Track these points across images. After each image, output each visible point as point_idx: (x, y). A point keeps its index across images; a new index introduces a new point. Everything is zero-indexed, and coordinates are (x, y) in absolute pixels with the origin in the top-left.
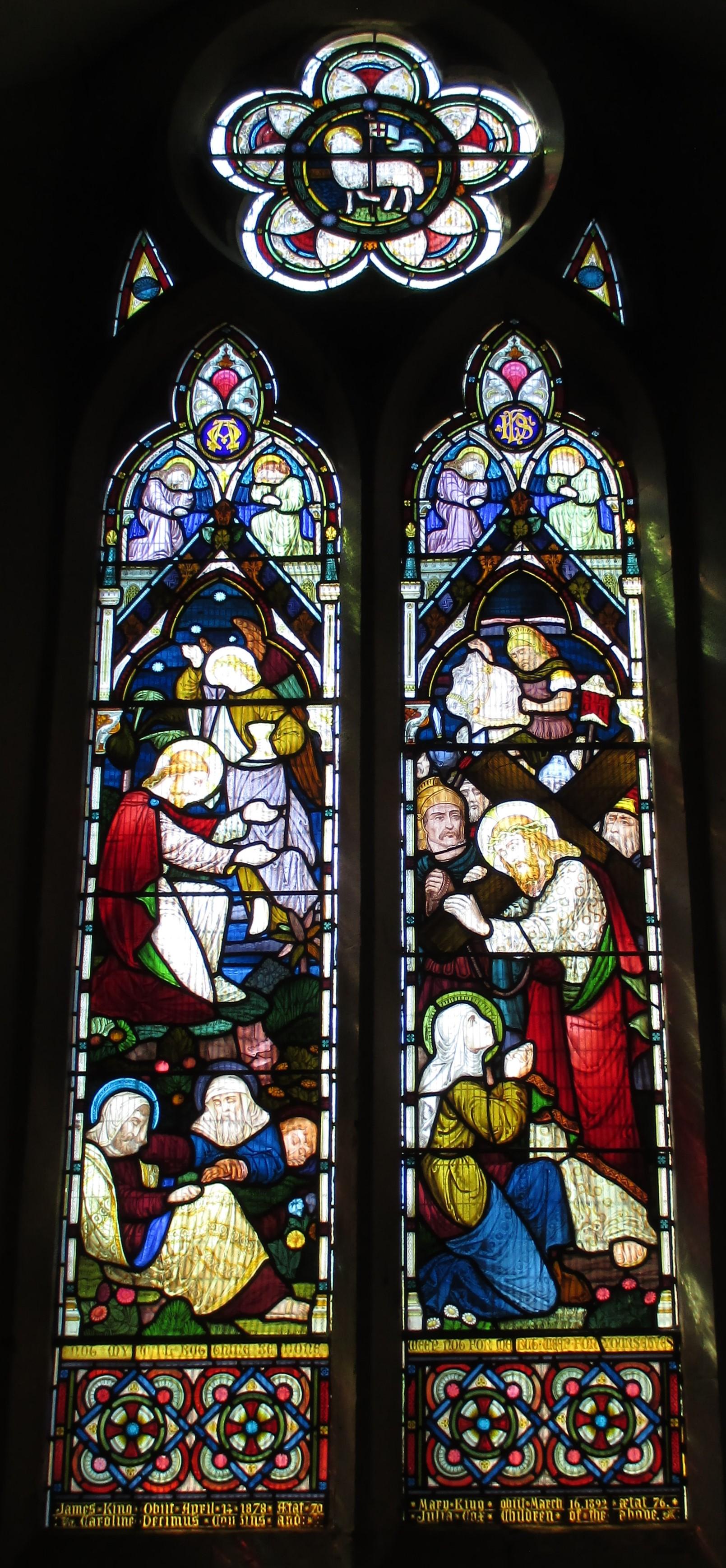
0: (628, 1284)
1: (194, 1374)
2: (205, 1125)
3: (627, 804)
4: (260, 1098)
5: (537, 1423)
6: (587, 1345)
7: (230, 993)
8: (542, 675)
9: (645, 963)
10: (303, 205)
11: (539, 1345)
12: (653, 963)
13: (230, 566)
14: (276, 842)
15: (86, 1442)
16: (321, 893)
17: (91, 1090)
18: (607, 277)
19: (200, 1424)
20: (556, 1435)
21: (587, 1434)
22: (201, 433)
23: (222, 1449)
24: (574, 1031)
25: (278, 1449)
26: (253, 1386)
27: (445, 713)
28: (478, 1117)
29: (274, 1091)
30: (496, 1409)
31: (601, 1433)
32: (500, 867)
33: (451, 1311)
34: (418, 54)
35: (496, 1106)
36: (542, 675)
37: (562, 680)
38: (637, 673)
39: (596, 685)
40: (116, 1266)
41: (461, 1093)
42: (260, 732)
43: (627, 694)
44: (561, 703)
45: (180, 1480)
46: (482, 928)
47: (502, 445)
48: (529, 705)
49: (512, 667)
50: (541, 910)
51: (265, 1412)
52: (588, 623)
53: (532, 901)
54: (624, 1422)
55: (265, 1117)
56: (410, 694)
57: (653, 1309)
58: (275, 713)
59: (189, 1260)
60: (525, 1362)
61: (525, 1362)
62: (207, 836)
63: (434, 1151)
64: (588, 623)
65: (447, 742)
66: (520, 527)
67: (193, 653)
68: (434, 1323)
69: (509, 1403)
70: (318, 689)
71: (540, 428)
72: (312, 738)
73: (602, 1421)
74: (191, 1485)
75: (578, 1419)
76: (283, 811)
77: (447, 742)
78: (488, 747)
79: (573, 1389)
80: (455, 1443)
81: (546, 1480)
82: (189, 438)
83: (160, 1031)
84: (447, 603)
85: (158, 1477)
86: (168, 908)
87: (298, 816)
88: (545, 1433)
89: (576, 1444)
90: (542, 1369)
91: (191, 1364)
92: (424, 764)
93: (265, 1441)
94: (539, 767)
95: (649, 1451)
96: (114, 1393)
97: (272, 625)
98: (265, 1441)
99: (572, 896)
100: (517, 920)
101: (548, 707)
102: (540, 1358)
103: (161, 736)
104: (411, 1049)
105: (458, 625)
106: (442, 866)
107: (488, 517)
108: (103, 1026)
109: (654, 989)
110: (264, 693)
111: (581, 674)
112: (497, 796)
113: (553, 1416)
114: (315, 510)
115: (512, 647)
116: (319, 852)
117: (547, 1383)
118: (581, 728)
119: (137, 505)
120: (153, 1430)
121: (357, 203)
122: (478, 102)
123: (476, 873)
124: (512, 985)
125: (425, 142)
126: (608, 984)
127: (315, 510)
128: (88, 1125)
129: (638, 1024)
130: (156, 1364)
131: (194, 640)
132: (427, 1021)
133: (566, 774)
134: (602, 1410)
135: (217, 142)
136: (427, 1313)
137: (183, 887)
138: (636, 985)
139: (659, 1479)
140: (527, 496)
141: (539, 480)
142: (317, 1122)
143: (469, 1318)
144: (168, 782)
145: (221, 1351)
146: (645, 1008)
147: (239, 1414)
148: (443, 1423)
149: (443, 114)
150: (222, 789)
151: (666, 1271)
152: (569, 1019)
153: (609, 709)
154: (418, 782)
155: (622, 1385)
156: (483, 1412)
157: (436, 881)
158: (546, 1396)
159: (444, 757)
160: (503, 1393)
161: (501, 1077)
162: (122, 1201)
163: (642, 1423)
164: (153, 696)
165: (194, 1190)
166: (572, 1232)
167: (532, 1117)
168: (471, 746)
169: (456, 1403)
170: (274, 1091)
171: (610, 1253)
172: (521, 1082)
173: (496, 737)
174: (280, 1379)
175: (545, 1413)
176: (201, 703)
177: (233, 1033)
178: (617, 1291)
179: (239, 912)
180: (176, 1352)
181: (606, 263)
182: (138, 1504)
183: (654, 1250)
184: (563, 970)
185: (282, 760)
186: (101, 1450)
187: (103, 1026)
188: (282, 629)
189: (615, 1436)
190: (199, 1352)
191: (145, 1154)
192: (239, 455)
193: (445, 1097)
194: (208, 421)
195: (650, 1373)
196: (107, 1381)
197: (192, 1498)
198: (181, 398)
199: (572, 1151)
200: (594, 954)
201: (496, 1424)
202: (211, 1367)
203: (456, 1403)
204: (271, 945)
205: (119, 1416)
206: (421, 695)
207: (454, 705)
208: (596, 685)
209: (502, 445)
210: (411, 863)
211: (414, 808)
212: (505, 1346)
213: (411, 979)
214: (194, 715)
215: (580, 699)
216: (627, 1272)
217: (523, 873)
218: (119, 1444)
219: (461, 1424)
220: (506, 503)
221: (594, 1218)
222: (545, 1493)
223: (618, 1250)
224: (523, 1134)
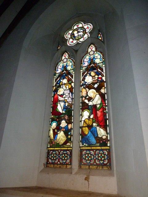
0: (104, 141)
1: (59, 151)
2: (61, 125)
3: (104, 88)
4: (66, 122)
5: (94, 157)
6: (99, 148)
7: (64, 112)
8: (94, 76)
9: (106, 104)
10: (72, 39)
11: (94, 148)
12: (106, 104)
13: (65, 72)
14: (68, 97)
15: (50, 158)
16: (72, 101)
17: (51, 123)
18: (101, 37)
19: (60, 156)
20: (96, 158)
21: (100, 158)
22: (63, 61)
23: (62, 159)
24: (98, 113)
25: (67, 159)
26: (65, 152)
27: (85, 82)
28: (87, 122)
29: (68, 122)
30: (90, 155)
31: (101, 158)
32: (90, 96)
33: (85, 144)
34: (82, 23)
35: (90, 121)
36: (94, 76)
37: (97, 76)
38: (104, 74)
39: (100, 76)
40: (53, 140)
41: (86, 120)
42: (67, 87)
43: (103, 76)
44: (96, 79)
45: (58, 162)
46: (88, 103)
47: (90, 55)
48: (93, 79)
49: (91, 76)
50: (94, 100)
51: (66, 155)
52: (99, 70)
53: (93, 99)
54: (104, 157)
55: (67, 124)
56: (81, 80)
57: (107, 144)
58: (69, 84)
59: (59, 139)
60: (93, 150)
61: (93, 150)
62: (62, 97)
63: (83, 127)
64: (99, 70)
65: (85, 85)
66: (92, 62)
67: (62, 80)
68: (83, 145)
69: (91, 154)
70: (73, 82)
71: (94, 52)
72: (72, 86)
73: (101, 157)
74: (59, 163)
75: (99, 157)
76: (69, 94)
77: (85, 85)
78: (89, 84)
79: (98, 153)
80: (85, 159)
81: (95, 164)
82: (62, 61)
83: (57, 116)
84: (85, 71)
85: (56, 162)
86: (59, 105)
87: (71, 94)
88: (95, 158)
89: (98, 160)
90: (95, 151)
91: (59, 150)
92: (82, 87)
93: (66, 158)
94: (94, 85)
95: (107, 161)
96: (52, 153)
97: (98, 70)
98: (66, 158)
99: (98, 98)
100: (92, 101)
101: (95, 79)
102: (94, 149)
103: (59, 88)
104: (81, 116)
105: (86, 73)
106: (84, 97)
107: (89, 62)
108: (53, 116)
109: (107, 107)
110: (68, 83)
111: (98, 75)
112: (90, 89)
113: (96, 156)
114: (73, 65)
115: (91, 74)
116: (72, 97)
117: (95, 152)
118: (99, 81)
119: (84, 61)
120: (56, 157)
121: (77, 37)
122: (87, 25)
123: (88, 97)
124: (91, 108)
125: (83, 30)
126: (101, 108)
127: (73, 65)
128: (51, 126)
129: (105, 111)
130: (56, 150)
131: (62, 79)
132: (83, 113)
133: (97, 86)
134: (101, 155)
135: (65, 37)
136: (82, 145)
137: (60, 102)
138: (105, 107)
139: (108, 164)
140: (93, 59)
141: (94, 57)
142: (72, 124)
143: (87, 145)
144: (59, 93)
145: (62, 149)
146: (106, 109)
147: (63, 155)
148: (84, 157)
149: (84, 27)
150: (64, 92)
151: (109, 139)
152: (97, 111)
153: (101, 78)
154: (82, 89)
155: (104, 153)
156: (88, 156)
157: (84, 98)
158: (95, 154)
159: (84, 86)
160: (90, 153)
161: (90, 118)
162: (53, 133)
163: (106, 157)
164: (58, 85)
165: (60, 132)
166: (98, 135)
167: (93, 122)
168: (87, 85)
169: (85, 154)
170: (68, 122)
171: (102, 137)
172: (92, 119)
173: (90, 83)
174: (68, 152)
175: (95, 156)
176: (62, 85)
177: (64, 116)
178: (103, 141)
179: (65, 104)
180: (58, 149)
181: (101, 35)
182: (54, 164)
183: (107, 137)
184: (96, 106)
185: (69, 89)
186: (51, 159)
187: (53, 116)
188: (70, 77)
189: (103, 159)
190: (60, 149)
191: (56, 128)
192: (66, 62)
193: (84, 121)
194: (90, 52)
195: (107, 151)
196: (52, 152)
197: (59, 164)
198: (62, 58)
199: (98, 126)
200: (100, 104)
201: (89, 157)
202: (61, 150)
203: (85, 154)
204: (68, 107)
205: (53, 155)
206: (82, 80)
207: (86, 81)
208: (100, 76)
209: (90, 55)
210: (81, 97)
211: (81, 92)
212: (90, 148)
213: (81, 109)
214: (61, 86)
215: (98, 78)
216: (104, 139)
217: (92, 96)
218: (52, 158)
219: (86, 157)
220: (91, 60)
221: (100, 133)
222: (95, 165)
223: (103, 137)
224: (92, 124)
